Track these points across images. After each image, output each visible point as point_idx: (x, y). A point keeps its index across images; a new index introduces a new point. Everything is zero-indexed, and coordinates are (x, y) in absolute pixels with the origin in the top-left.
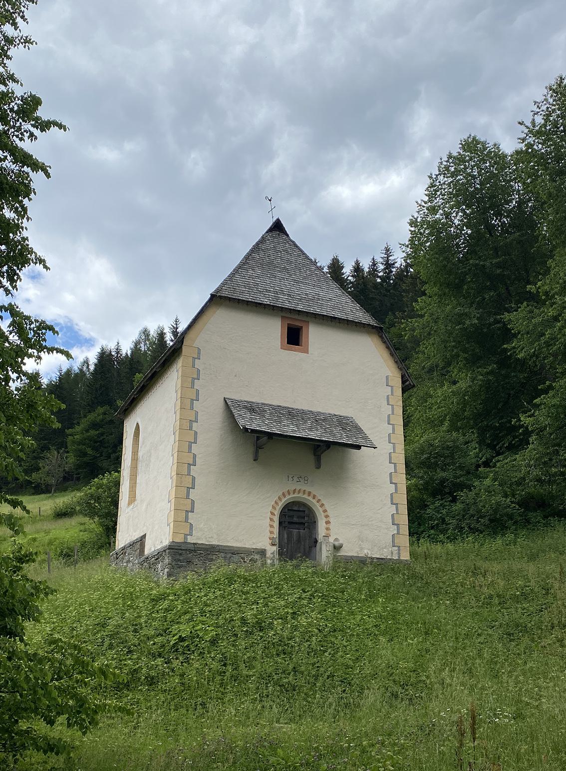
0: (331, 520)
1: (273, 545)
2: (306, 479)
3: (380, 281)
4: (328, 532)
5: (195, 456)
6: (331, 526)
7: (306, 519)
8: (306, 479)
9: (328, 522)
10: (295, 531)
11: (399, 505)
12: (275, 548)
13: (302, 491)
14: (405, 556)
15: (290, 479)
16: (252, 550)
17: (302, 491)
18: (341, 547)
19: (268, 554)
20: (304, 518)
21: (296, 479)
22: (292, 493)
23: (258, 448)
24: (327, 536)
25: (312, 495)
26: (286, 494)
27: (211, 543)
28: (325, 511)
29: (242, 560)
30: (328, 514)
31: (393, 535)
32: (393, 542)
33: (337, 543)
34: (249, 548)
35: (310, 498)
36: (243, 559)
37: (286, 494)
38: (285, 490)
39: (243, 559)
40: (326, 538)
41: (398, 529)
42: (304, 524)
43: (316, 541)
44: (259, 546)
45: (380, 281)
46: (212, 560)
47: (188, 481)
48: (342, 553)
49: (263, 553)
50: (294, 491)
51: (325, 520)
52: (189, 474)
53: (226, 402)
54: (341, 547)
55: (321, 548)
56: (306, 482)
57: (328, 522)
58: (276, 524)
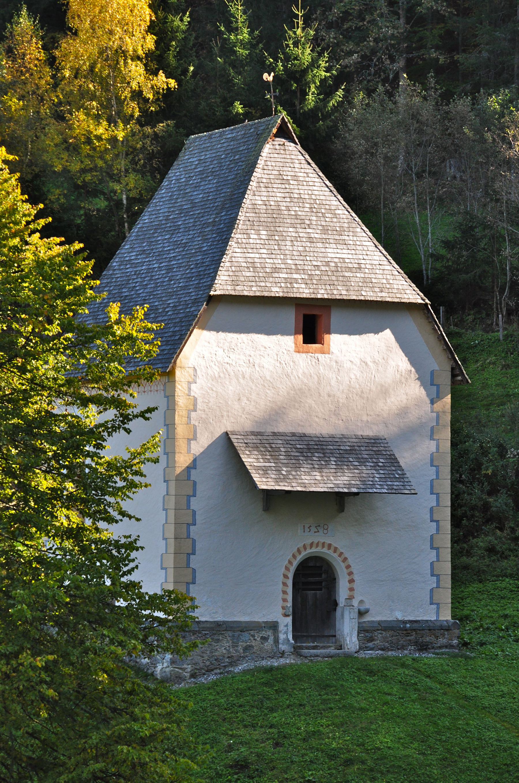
0: (356, 577)
1: (286, 615)
2: (326, 527)
3: (237, 104)
4: (351, 593)
5: (194, 513)
6: (355, 585)
7: (324, 576)
8: (326, 527)
9: (351, 581)
10: (310, 593)
11: (440, 550)
12: (289, 620)
13: (320, 545)
14: (446, 616)
15: (307, 530)
16: (263, 625)
17: (320, 545)
18: (367, 611)
19: (281, 628)
20: (320, 575)
21: (313, 529)
22: (308, 547)
23: (267, 508)
24: (351, 598)
25: (332, 548)
26: (302, 549)
27: (216, 620)
28: (348, 567)
29: (252, 639)
30: (352, 570)
31: (432, 590)
32: (431, 598)
33: (362, 608)
34: (258, 622)
35: (331, 552)
36: (253, 636)
37: (302, 549)
38: (301, 545)
39: (253, 636)
40: (348, 601)
41: (438, 582)
42: (322, 582)
43: (336, 604)
44: (270, 618)
45: (237, 104)
46: (218, 641)
47: (187, 547)
48: (367, 618)
49: (274, 626)
50: (311, 545)
51: (343, 565)
52: (188, 537)
53: (229, 439)
54: (367, 611)
55: (343, 615)
56: (325, 531)
57: (351, 581)
58: (290, 590)
